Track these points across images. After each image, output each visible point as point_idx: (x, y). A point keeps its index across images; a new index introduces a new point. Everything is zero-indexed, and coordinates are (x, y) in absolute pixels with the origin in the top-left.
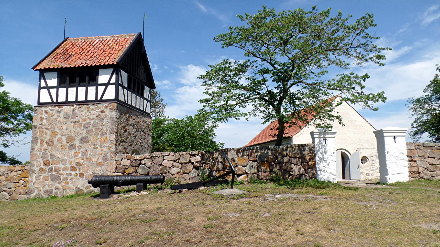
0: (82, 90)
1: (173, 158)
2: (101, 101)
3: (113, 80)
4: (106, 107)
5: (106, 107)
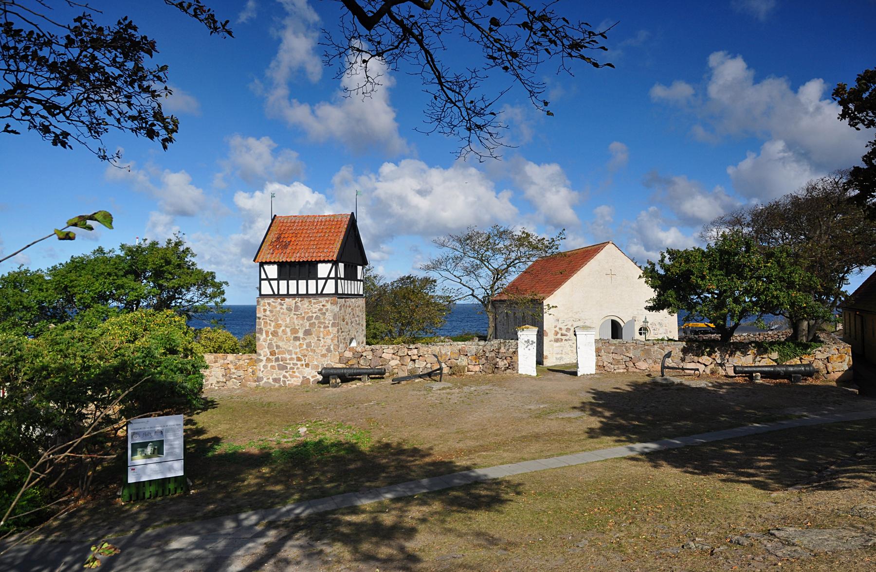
0: (302, 283)
1: (392, 351)
2: (322, 295)
3: (333, 275)
4: (327, 302)
5: (327, 302)
